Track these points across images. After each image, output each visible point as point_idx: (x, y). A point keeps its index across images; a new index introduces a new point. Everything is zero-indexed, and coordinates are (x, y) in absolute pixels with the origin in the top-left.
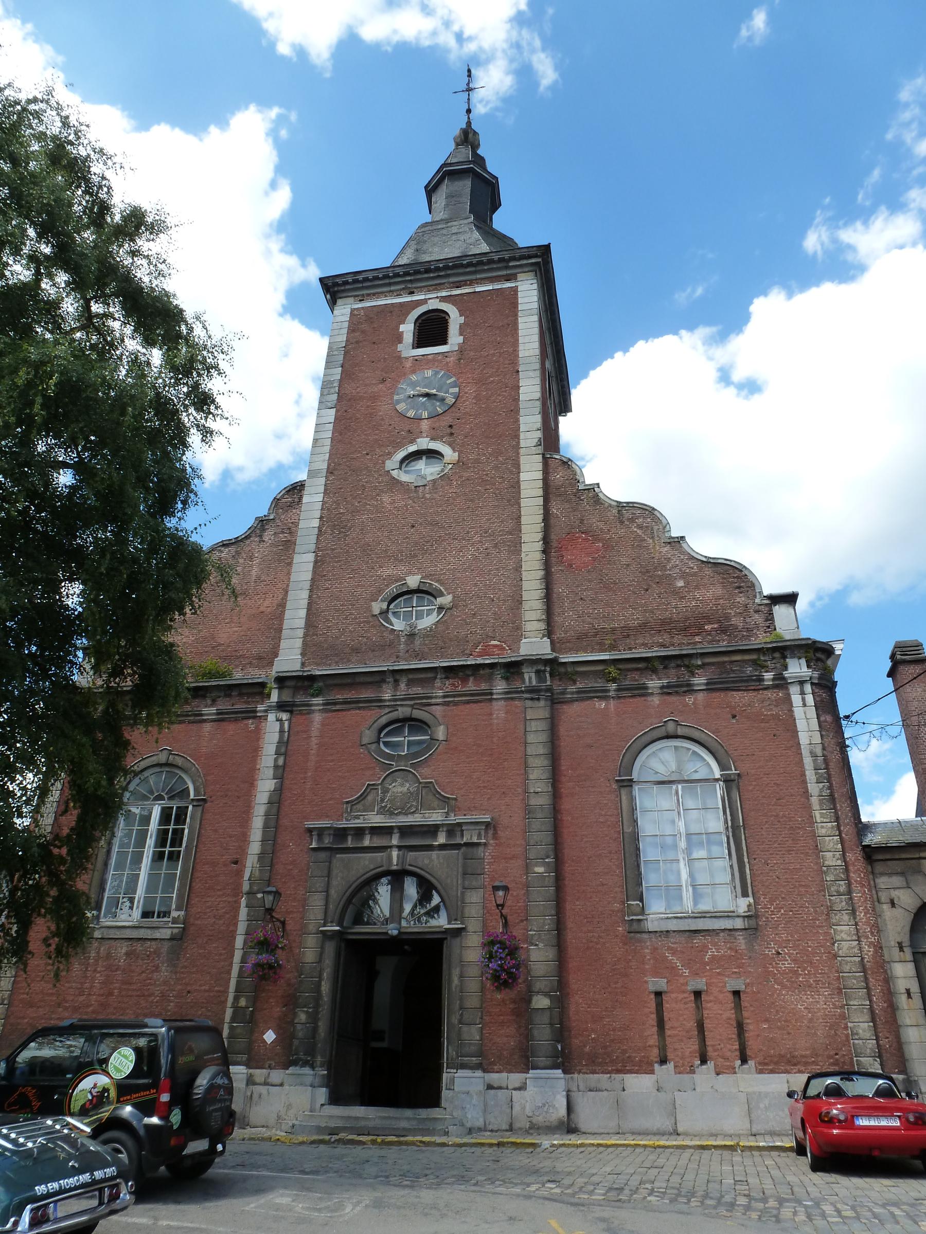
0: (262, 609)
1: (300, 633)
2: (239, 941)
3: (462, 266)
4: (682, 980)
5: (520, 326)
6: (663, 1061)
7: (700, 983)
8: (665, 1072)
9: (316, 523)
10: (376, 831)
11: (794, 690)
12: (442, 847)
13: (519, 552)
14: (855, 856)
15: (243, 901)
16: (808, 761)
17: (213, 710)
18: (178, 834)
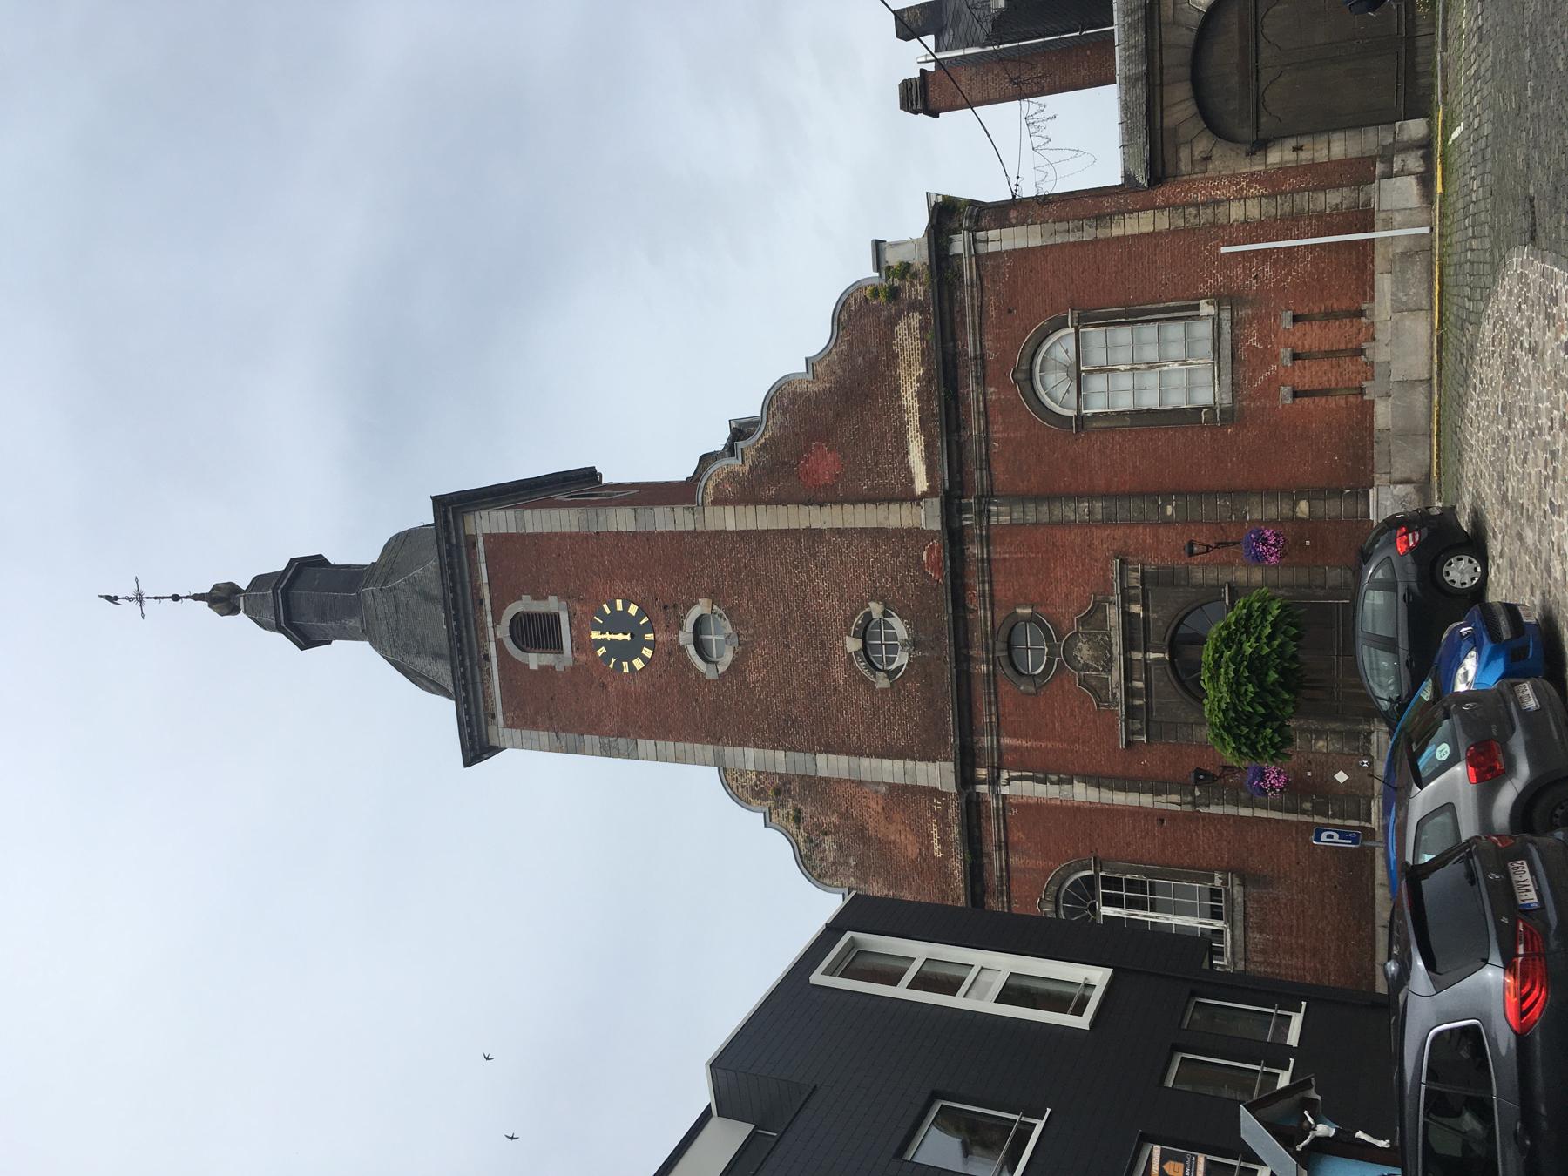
0: (879, 809)
1: (910, 764)
2: (1245, 812)
3: (455, 600)
4: (1282, 372)
5: (538, 530)
6: (1362, 391)
7: (1286, 353)
8: (1372, 390)
9: (780, 754)
10: (1128, 677)
11: (982, 248)
12: (1145, 608)
13: (820, 532)
14: (1159, 195)
15: (1204, 810)
16: (1059, 239)
17: (996, 855)
18: (1131, 885)
